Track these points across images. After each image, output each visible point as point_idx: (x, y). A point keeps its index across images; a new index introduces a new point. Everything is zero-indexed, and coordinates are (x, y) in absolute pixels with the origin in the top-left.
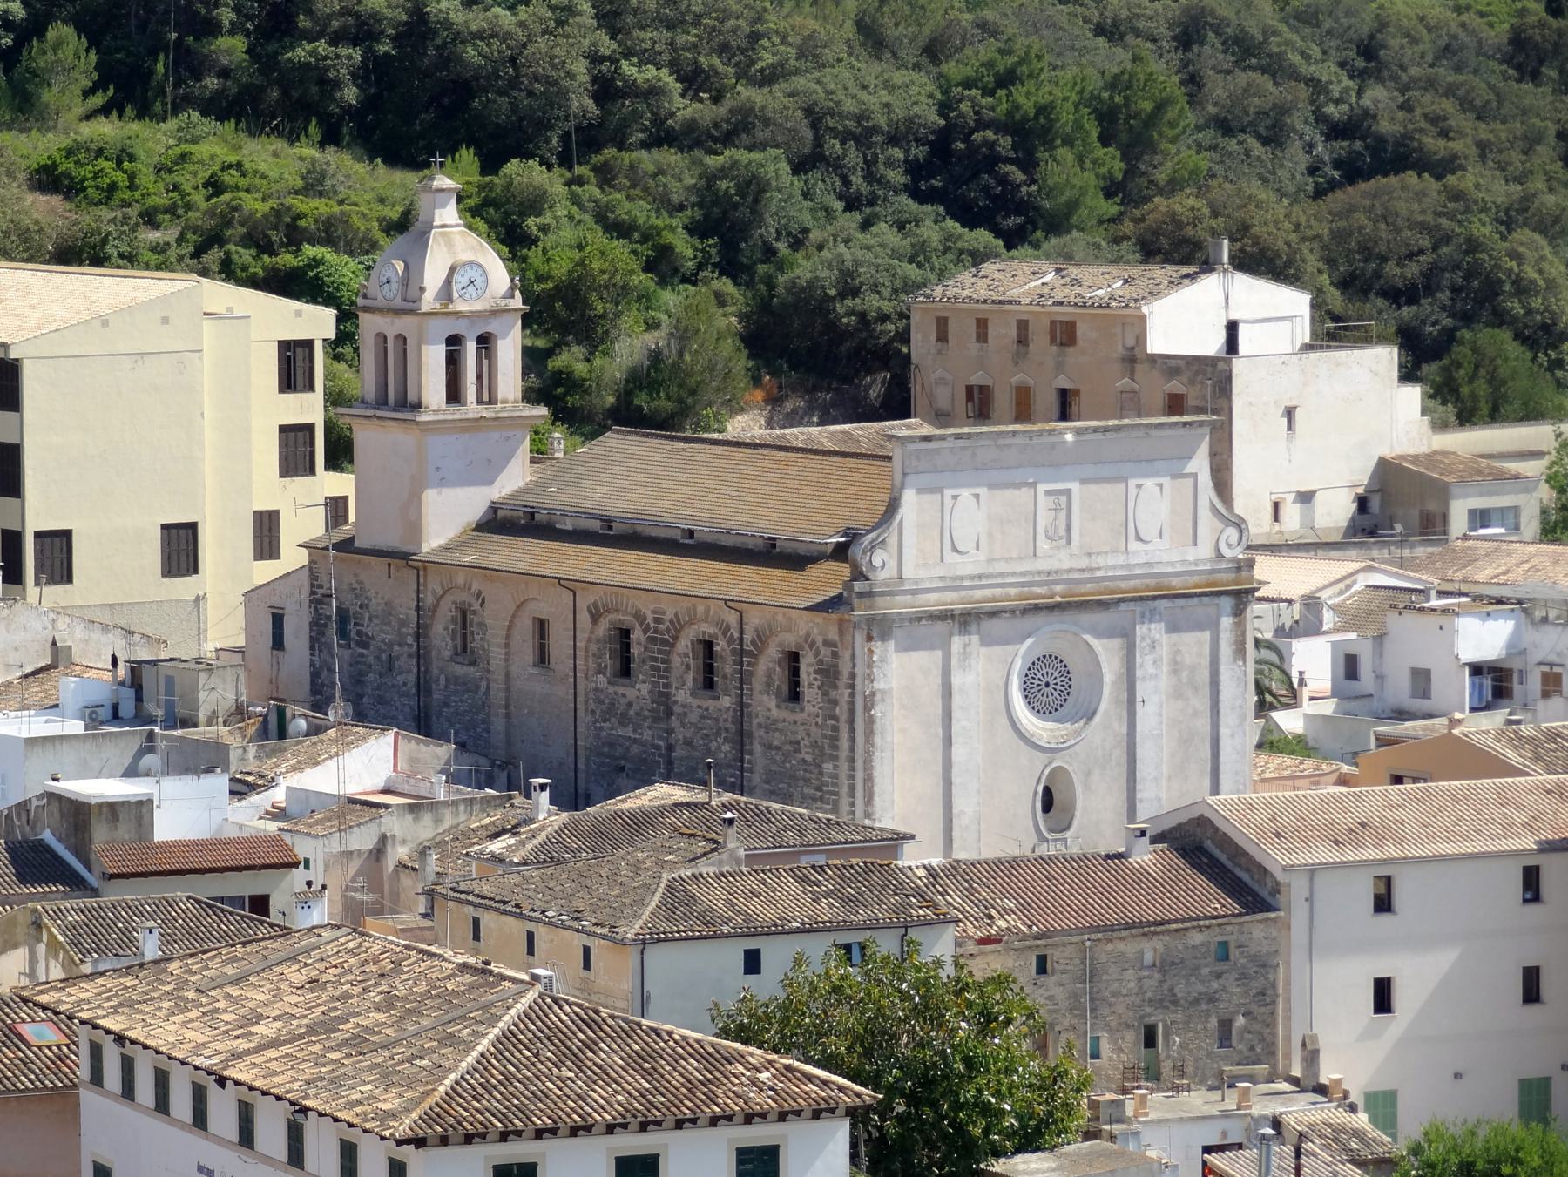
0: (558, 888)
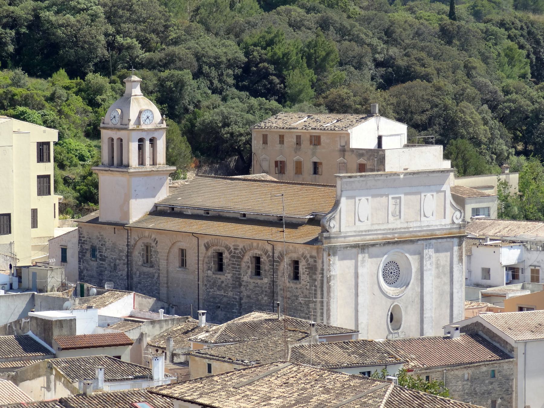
0: (244, 352)
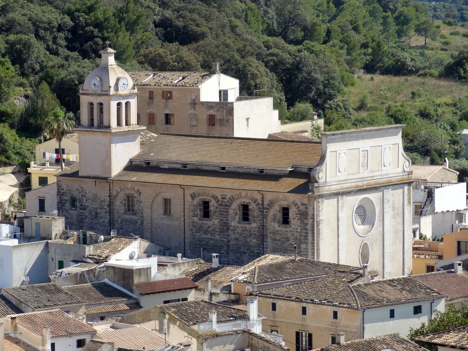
0: (307, 292)
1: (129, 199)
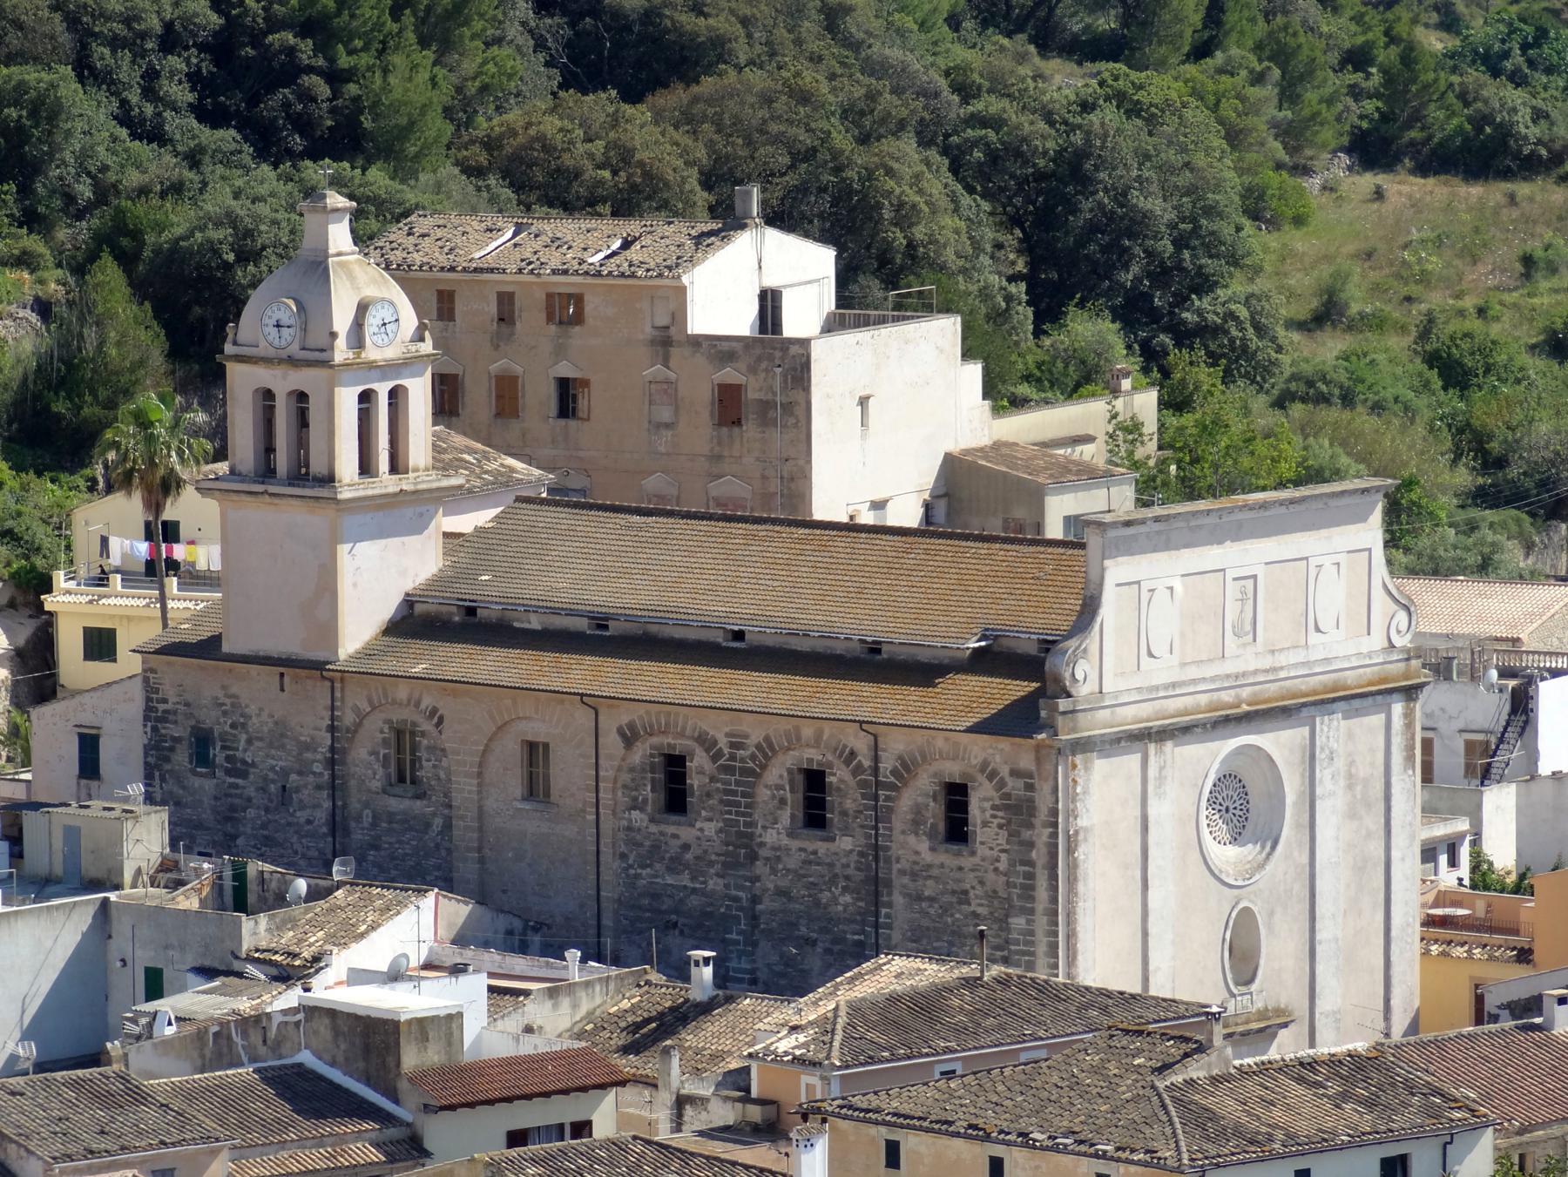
0: (1008, 1103)
1: (403, 739)
